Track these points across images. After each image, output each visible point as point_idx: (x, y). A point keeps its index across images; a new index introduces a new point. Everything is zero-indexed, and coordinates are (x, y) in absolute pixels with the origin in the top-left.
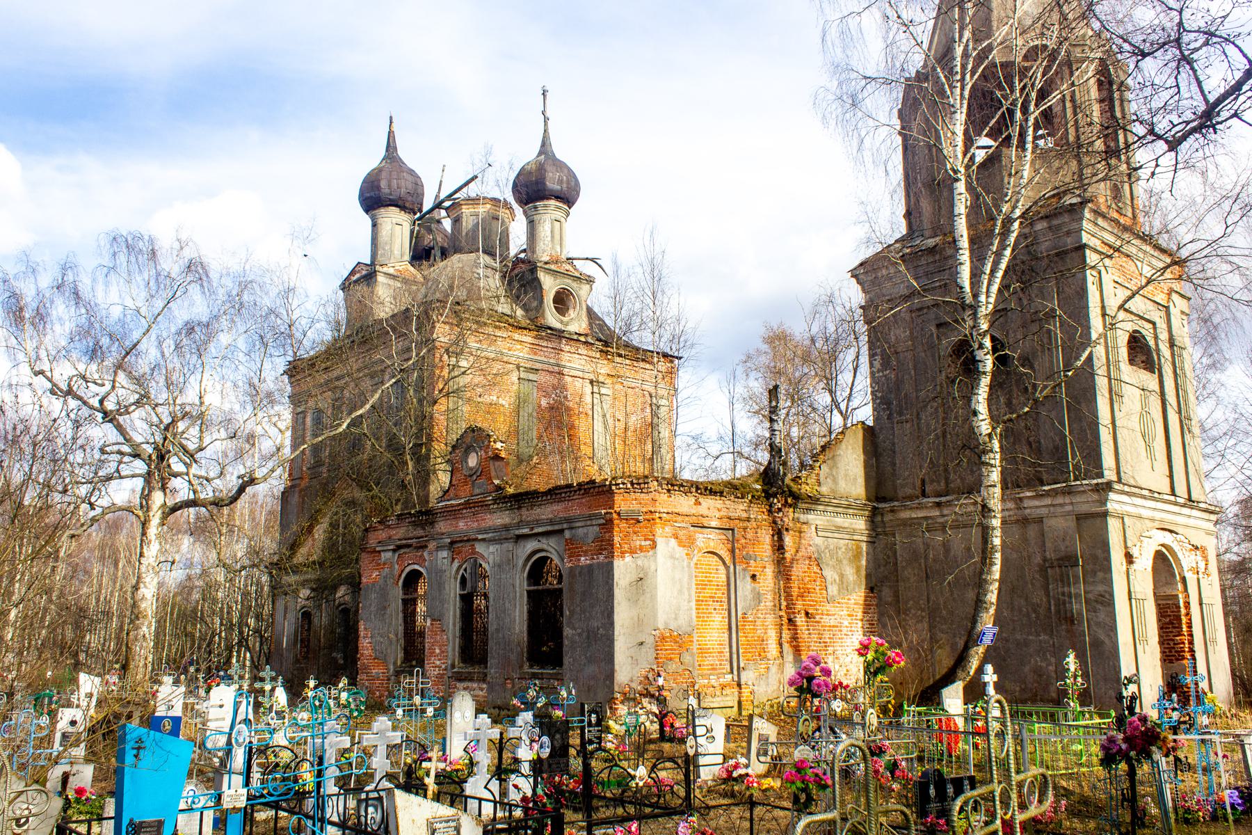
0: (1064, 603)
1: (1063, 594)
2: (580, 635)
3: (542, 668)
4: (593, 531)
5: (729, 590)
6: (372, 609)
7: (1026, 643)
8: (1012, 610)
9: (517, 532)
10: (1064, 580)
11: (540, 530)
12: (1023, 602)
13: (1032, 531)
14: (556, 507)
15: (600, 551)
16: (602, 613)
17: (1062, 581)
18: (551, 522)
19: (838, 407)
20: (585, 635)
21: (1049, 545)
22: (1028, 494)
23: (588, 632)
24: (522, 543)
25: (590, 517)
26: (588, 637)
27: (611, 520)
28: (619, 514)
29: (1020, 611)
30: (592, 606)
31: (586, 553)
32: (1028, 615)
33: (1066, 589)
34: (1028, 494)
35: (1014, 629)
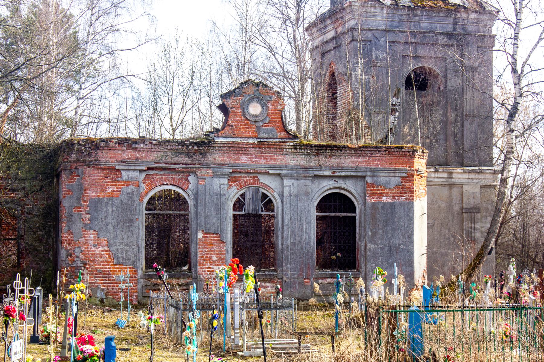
0: (471, 233)
1: (471, 228)
2: (381, 248)
3: (333, 271)
4: (395, 180)
5: (283, 213)
6: (110, 220)
7: (447, 254)
8: (440, 235)
9: (317, 173)
10: (473, 221)
11: (343, 174)
12: (447, 231)
13: (455, 191)
14: (356, 159)
15: (401, 194)
16: (404, 235)
17: (471, 221)
18: (356, 170)
19: (28, 60)
20: (387, 249)
21: (465, 199)
22: (459, 171)
23: (390, 247)
24: (316, 182)
25: (395, 171)
26: (390, 250)
27: (412, 175)
28: (417, 171)
29: (445, 236)
30: (394, 230)
31: (387, 194)
32: (449, 239)
33: (473, 225)
34: (459, 171)
35: (440, 247)
